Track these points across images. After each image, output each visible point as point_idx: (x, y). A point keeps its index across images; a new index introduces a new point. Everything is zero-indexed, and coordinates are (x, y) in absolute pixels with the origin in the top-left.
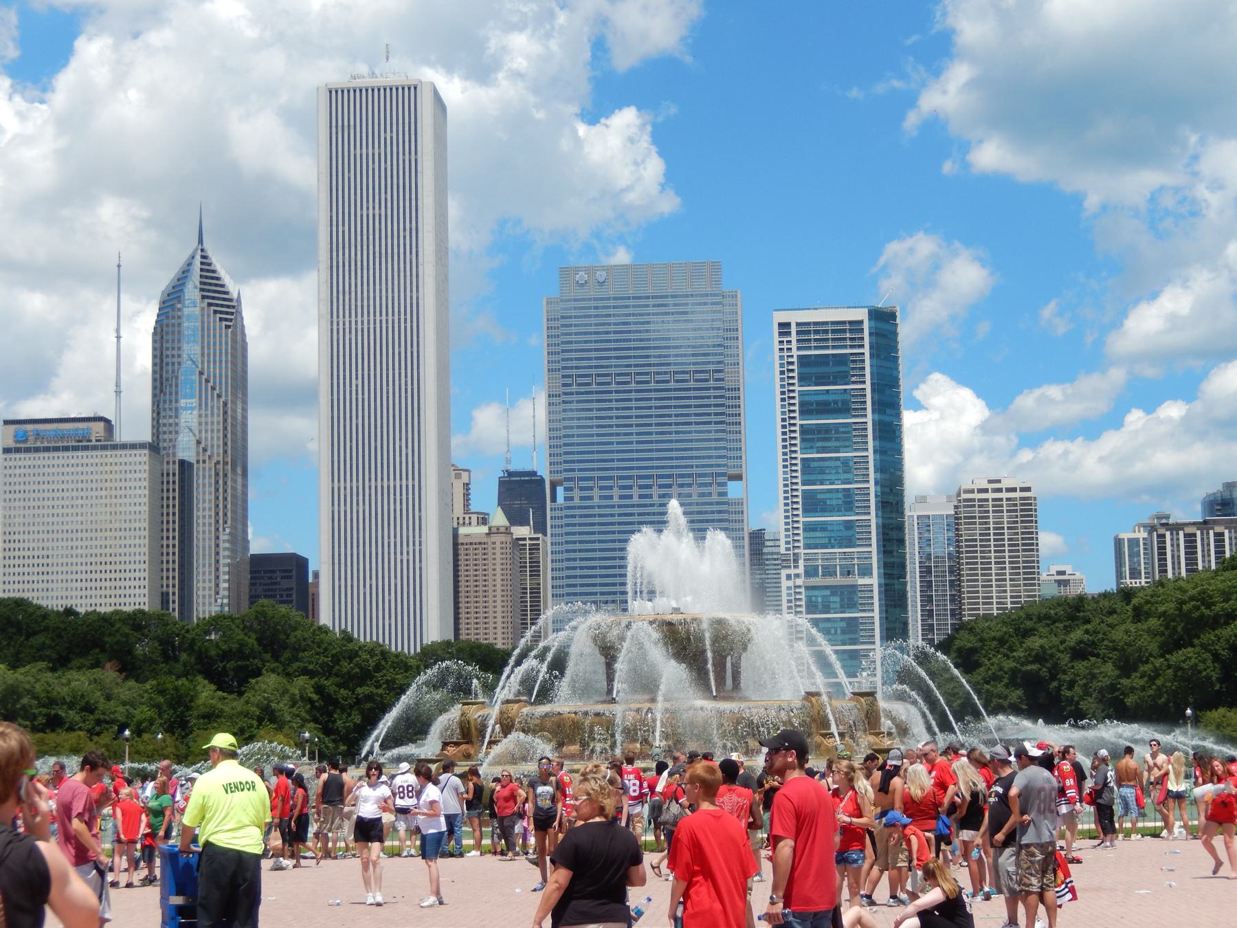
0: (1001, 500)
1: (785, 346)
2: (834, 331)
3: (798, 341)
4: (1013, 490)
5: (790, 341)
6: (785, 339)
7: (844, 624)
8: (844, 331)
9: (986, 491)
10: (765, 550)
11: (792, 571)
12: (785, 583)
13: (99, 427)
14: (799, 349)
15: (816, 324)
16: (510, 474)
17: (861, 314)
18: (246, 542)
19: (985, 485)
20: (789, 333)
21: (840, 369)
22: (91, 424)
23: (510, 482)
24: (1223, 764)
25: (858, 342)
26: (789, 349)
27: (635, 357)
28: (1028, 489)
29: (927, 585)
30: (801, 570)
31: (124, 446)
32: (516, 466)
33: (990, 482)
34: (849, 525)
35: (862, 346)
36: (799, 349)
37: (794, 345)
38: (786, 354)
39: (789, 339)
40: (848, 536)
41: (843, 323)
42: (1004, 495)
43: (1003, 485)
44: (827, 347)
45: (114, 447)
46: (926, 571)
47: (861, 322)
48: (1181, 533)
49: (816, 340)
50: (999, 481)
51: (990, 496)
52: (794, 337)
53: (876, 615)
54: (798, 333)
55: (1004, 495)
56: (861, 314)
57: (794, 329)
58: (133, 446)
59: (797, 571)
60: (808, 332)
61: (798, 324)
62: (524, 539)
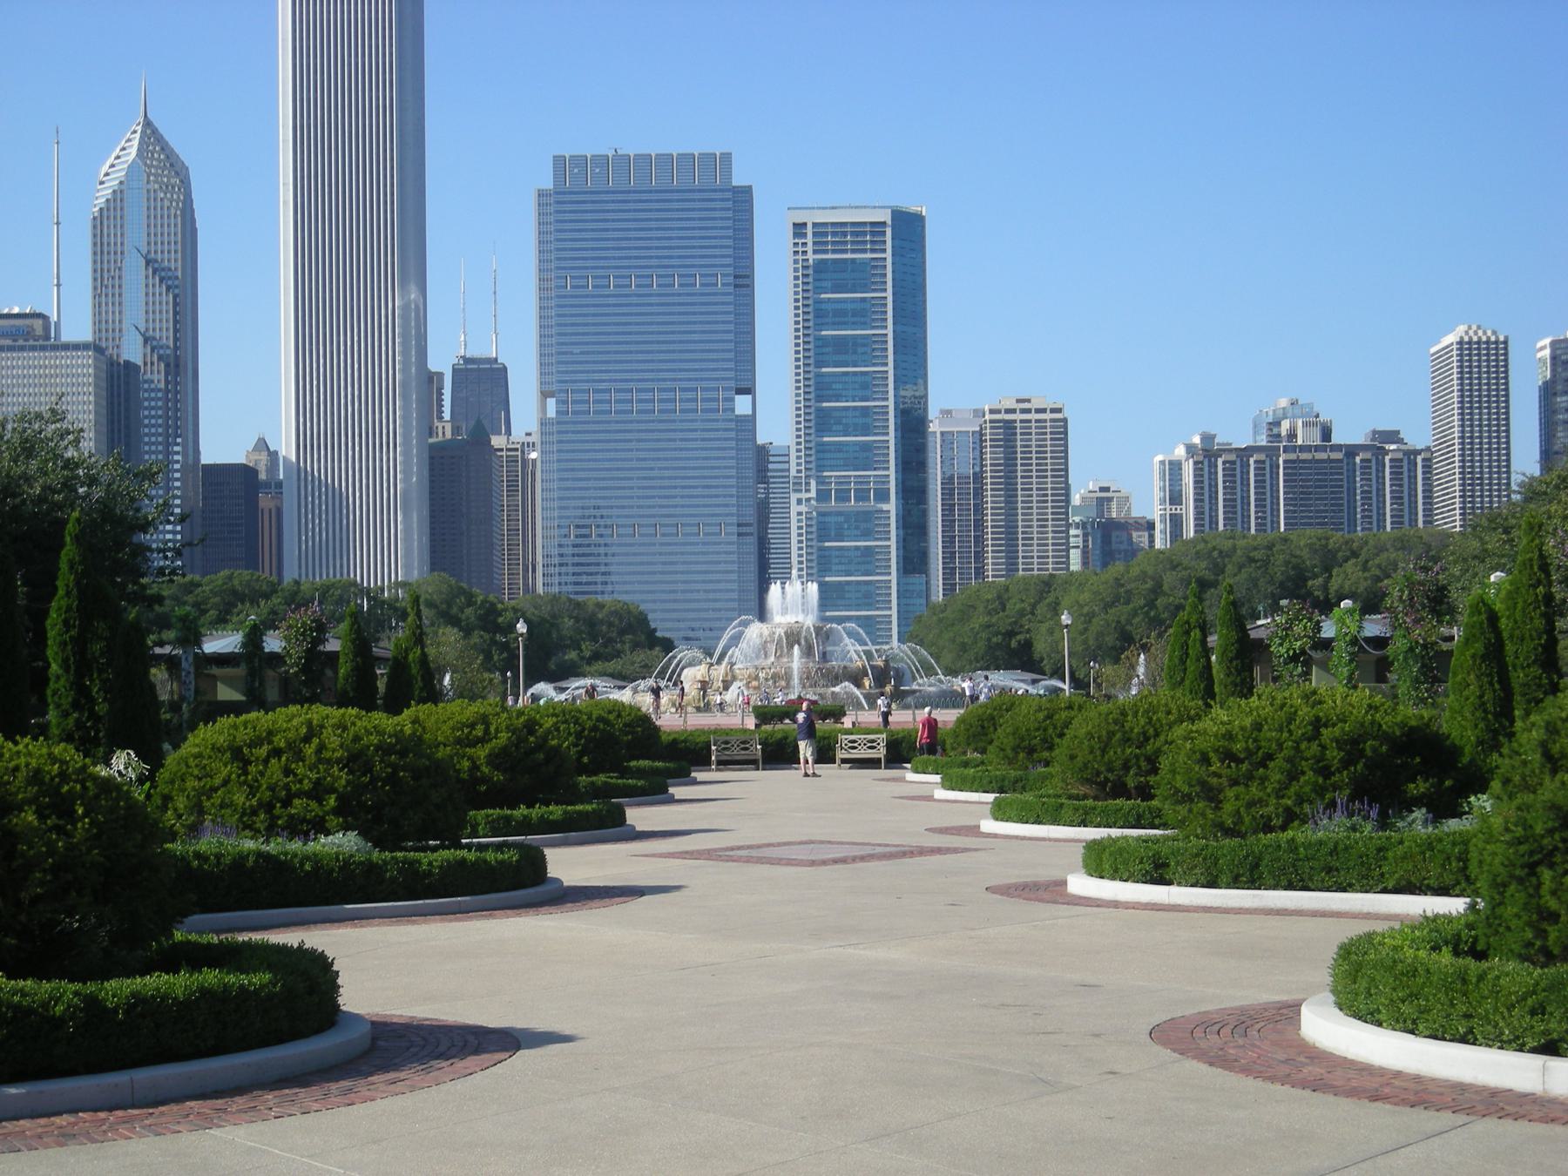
0: (1030, 421)
1: (800, 249)
2: (853, 233)
3: (814, 243)
4: (1043, 411)
5: (806, 243)
6: (800, 241)
7: (913, 738)
8: (865, 234)
9: (1013, 411)
10: (771, 466)
11: (804, 496)
12: (794, 509)
13: (38, 324)
14: (815, 252)
15: (833, 224)
16: (467, 360)
17: (885, 216)
18: (197, 452)
19: (1011, 404)
20: (804, 236)
21: (863, 276)
22: (28, 322)
23: (467, 369)
24: (184, 619)
25: (878, 246)
26: (805, 253)
27: (614, 230)
28: (1059, 410)
29: (948, 509)
30: (813, 494)
31: (66, 347)
32: (475, 352)
33: (1018, 401)
34: (866, 447)
35: (886, 364)
36: (815, 252)
37: (810, 248)
38: (800, 257)
39: (803, 241)
40: (866, 457)
41: (864, 224)
42: (1033, 416)
43: (1034, 405)
44: (845, 251)
45: (55, 348)
46: (948, 492)
47: (884, 224)
48: (1220, 461)
49: (833, 243)
50: (1029, 401)
51: (1018, 416)
52: (810, 239)
53: (891, 438)
54: (814, 234)
55: (1033, 416)
56: (885, 216)
57: (810, 226)
58: (76, 347)
59: (799, 495)
60: (826, 234)
61: (815, 225)
62: (502, 450)
